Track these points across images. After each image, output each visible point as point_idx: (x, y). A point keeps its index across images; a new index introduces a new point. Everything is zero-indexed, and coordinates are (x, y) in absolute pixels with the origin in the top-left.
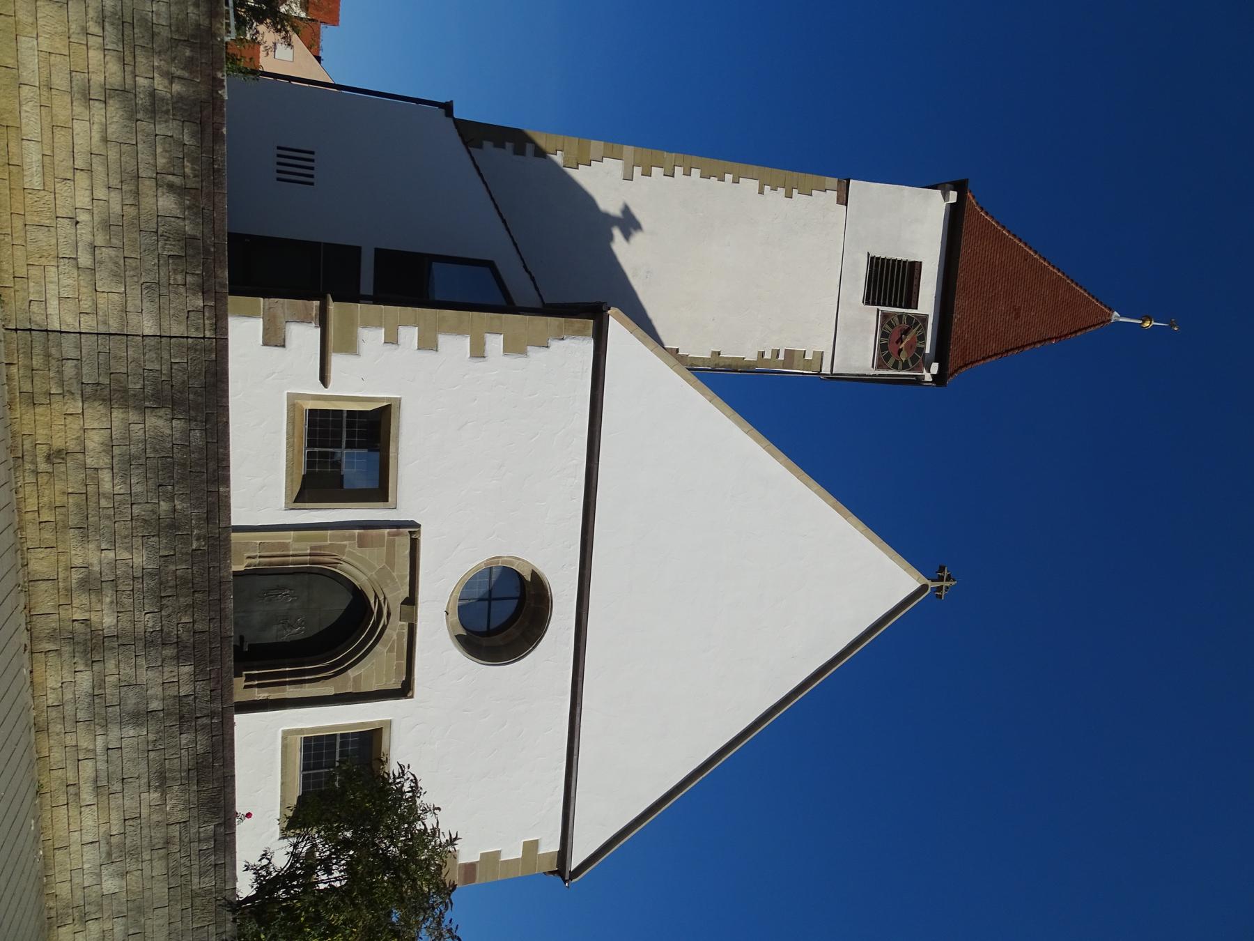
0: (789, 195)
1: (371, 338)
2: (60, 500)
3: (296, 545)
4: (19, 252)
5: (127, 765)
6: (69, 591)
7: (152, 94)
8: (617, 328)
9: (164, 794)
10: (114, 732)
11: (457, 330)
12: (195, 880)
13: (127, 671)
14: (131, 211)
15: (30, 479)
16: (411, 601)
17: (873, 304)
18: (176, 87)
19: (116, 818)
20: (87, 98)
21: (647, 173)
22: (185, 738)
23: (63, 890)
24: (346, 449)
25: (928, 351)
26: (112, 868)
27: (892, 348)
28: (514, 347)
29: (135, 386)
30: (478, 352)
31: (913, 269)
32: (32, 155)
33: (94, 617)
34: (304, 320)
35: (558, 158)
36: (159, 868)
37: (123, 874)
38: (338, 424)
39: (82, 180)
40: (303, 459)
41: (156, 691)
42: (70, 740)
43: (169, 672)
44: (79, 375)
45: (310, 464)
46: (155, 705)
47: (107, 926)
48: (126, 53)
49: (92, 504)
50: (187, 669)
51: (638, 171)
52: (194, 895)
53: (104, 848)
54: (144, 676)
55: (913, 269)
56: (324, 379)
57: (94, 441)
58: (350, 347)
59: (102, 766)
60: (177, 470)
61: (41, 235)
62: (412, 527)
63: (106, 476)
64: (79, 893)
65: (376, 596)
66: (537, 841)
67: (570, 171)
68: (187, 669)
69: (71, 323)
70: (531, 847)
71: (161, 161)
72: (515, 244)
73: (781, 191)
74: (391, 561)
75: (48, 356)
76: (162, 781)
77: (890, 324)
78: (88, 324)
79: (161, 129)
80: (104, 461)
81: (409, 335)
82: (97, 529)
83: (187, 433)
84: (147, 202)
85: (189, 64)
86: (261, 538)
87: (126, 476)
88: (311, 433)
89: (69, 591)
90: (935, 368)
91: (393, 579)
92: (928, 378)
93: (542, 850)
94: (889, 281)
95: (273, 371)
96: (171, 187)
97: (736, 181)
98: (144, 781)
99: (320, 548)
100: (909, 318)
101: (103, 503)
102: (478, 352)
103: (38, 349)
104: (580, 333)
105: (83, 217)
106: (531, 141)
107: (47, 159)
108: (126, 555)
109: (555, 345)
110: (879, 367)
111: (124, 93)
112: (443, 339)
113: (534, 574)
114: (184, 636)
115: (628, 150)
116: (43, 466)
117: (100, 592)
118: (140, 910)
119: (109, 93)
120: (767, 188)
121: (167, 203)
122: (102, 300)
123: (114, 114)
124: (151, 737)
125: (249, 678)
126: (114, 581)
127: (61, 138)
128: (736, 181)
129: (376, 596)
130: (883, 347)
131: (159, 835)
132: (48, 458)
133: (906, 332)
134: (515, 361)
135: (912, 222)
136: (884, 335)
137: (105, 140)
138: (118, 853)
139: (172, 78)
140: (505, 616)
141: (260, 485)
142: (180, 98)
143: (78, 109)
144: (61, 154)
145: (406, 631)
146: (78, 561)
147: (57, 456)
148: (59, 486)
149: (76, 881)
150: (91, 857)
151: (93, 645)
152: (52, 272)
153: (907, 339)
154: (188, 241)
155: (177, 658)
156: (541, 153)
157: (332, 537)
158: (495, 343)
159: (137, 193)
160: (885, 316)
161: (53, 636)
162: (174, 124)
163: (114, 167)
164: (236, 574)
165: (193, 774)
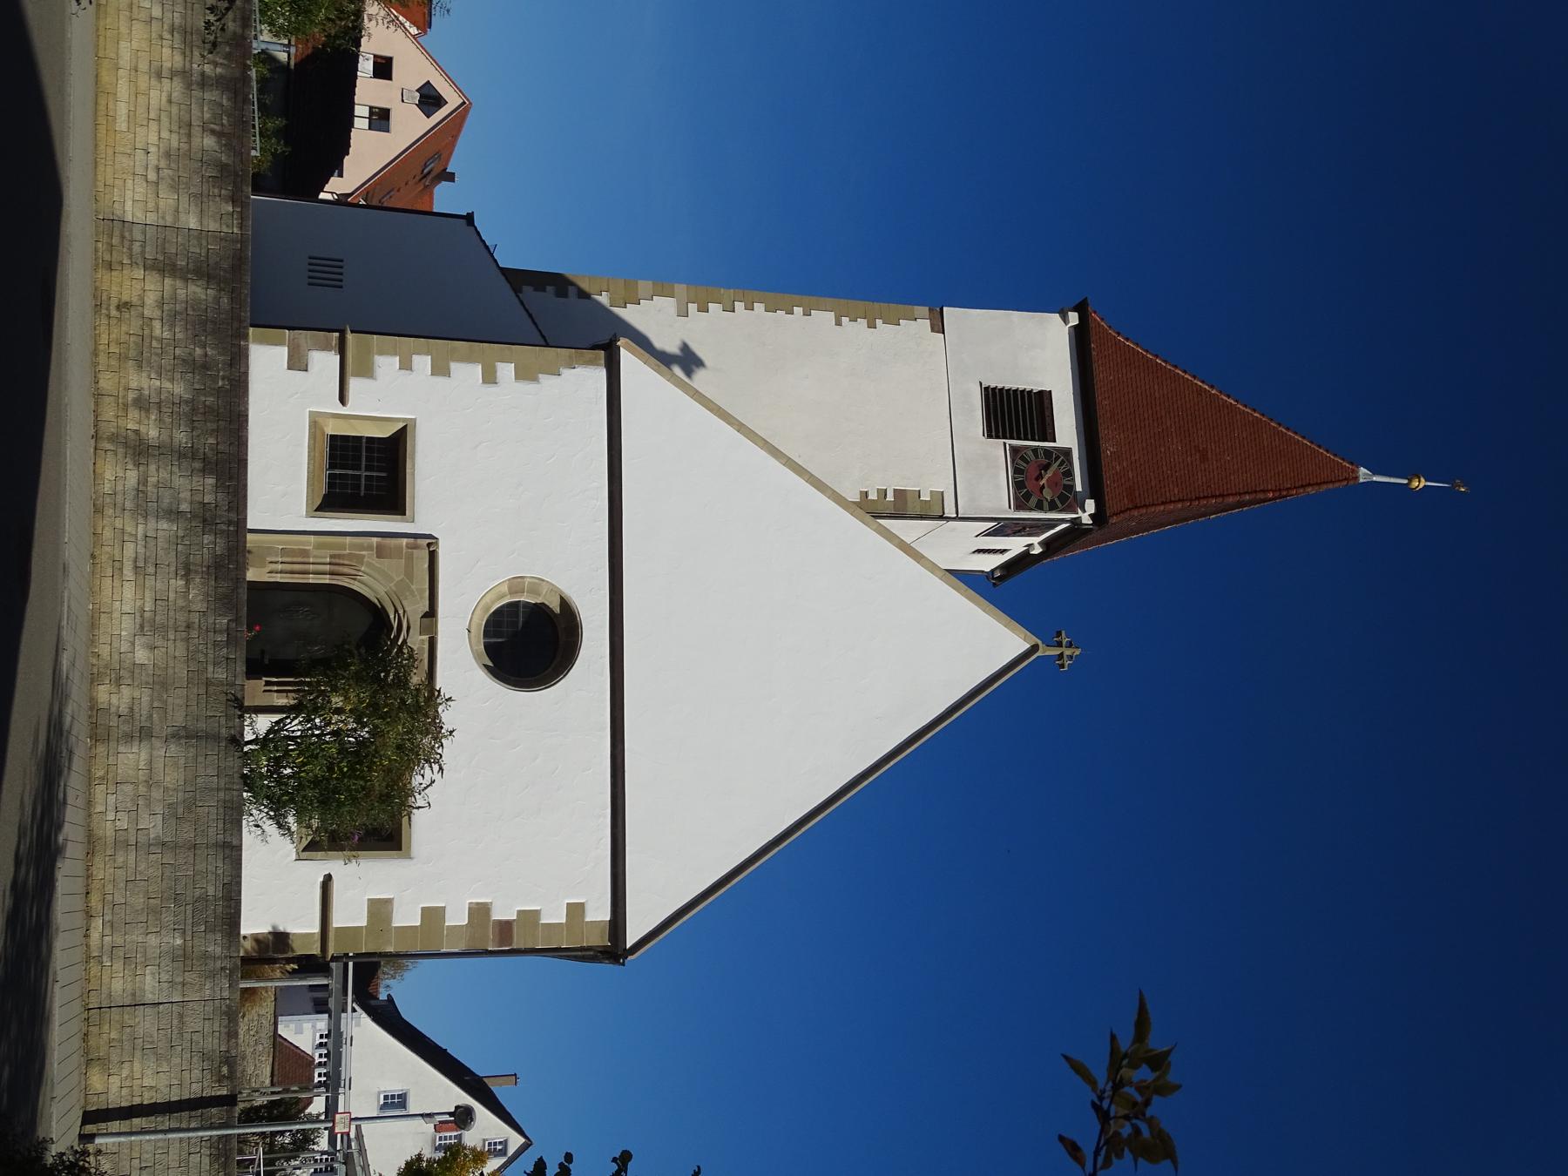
0: (872, 325)
1: (386, 364)
2: (124, 338)
3: (316, 552)
4: (109, 169)
5: (161, 553)
6: (126, 406)
7: (203, 74)
8: (629, 360)
9: (188, 582)
10: (152, 524)
11: (468, 359)
12: (210, 669)
13: (164, 474)
14: (184, 146)
15: (104, 321)
16: (431, 613)
17: (997, 437)
18: (219, 70)
19: (149, 595)
20: (159, 76)
21: (704, 309)
22: (207, 539)
23: (104, 651)
24: (367, 472)
25: (1079, 488)
26: (144, 639)
27: (1030, 485)
28: (525, 374)
29: (181, 263)
30: (490, 378)
31: (1042, 401)
32: (122, 110)
33: (143, 429)
34: (326, 347)
35: (604, 299)
36: (180, 651)
37: (153, 648)
38: (357, 449)
39: (153, 126)
40: (324, 480)
41: (185, 495)
42: (118, 523)
43: (197, 482)
44: (143, 252)
45: (331, 485)
46: (184, 507)
47: (137, 694)
48: (187, 48)
49: (146, 344)
50: (211, 481)
51: (692, 307)
52: (208, 683)
53: (138, 620)
54: (178, 482)
55: (1042, 401)
56: (343, 399)
57: (151, 299)
58: (367, 371)
59: (141, 550)
60: (209, 326)
61: (125, 160)
62: (431, 545)
63: (157, 324)
64: (116, 657)
65: (396, 611)
66: (582, 905)
67: (616, 310)
68: (211, 481)
69: (140, 217)
70: (576, 910)
71: (207, 116)
72: (530, 316)
73: (862, 322)
74: (409, 574)
75: (123, 237)
76: (187, 572)
77: (1022, 458)
78: (151, 218)
79: (207, 96)
80: (157, 313)
81: (423, 363)
82: (149, 362)
83: (217, 300)
84: (196, 141)
85: (228, 56)
86: (280, 543)
87: (172, 326)
88: (332, 456)
89: (126, 406)
90: (1090, 505)
91: (412, 592)
92: (1086, 519)
93: (590, 917)
94: (1014, 413)
95: (292, 397)
96: (213, 132)
97: (807, 314)
98: (173, 569)
99: (339, 556)
100: (1047, 452)
101: (155, 344)
102: (490, 378)
103: (117, 233)
104: (592, 362)
105: (152, 149)
106: (572, 284)
107: (131, 116)
108: (168, 385)
109: (567, 373)
110: (1019, 507)
111: (184, 74)
112: (454, 366)
113: (565, 604)
114: (210, 454)
115: (680, 289)
116: (114, 313)
117: (148, 411)
118: (164, 685)
119: (173, 74)
120: (845, 320)
121: (209, 142)
122: (162, 203)
123: (177, 87)
124: (181, 533)
125: (268, 683)
126: (159, 404)
127: (141, 99)
128: (807, 314)
129: (396, 611)
130: (1019, 485)
131: (182, 618)
132: (118, 308)
133: (1046, 467)
134: (527, 387)
135: (1036, 350)
136: (1017, 471)
137: (170, 101)
138: (147, 626)
139: (216, 64)
140: (530, 643)
141: (280, 492)
142: (221, 76)
143: (154, 82)
144: (141, 110)
145: (426, 646)
146: (134, 385)
147: (124, 306)
148: (124, 328)
149: (115, 645)
150: (127, 627)
151: (139, 450)
152: (129, 183)
153: (1049, 474)
154: (223, 168)
155: (203, 472)
156: (584, 295)
157: (353, 546)
158: (506, 370)
159: (189, 135)
160: (1015, 450)
161: (113, 438)
162: (216, 93)
163: (175, 118)
164: (255, 586)
165: (212, 570)
